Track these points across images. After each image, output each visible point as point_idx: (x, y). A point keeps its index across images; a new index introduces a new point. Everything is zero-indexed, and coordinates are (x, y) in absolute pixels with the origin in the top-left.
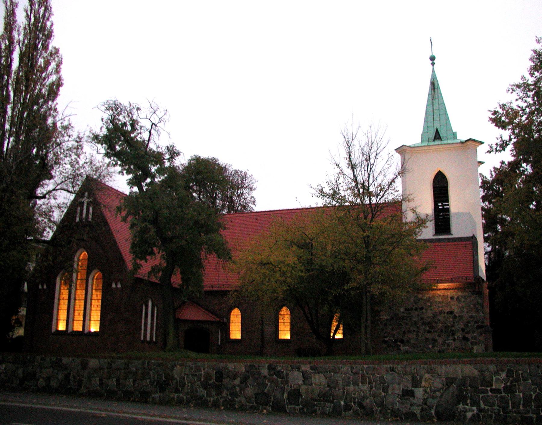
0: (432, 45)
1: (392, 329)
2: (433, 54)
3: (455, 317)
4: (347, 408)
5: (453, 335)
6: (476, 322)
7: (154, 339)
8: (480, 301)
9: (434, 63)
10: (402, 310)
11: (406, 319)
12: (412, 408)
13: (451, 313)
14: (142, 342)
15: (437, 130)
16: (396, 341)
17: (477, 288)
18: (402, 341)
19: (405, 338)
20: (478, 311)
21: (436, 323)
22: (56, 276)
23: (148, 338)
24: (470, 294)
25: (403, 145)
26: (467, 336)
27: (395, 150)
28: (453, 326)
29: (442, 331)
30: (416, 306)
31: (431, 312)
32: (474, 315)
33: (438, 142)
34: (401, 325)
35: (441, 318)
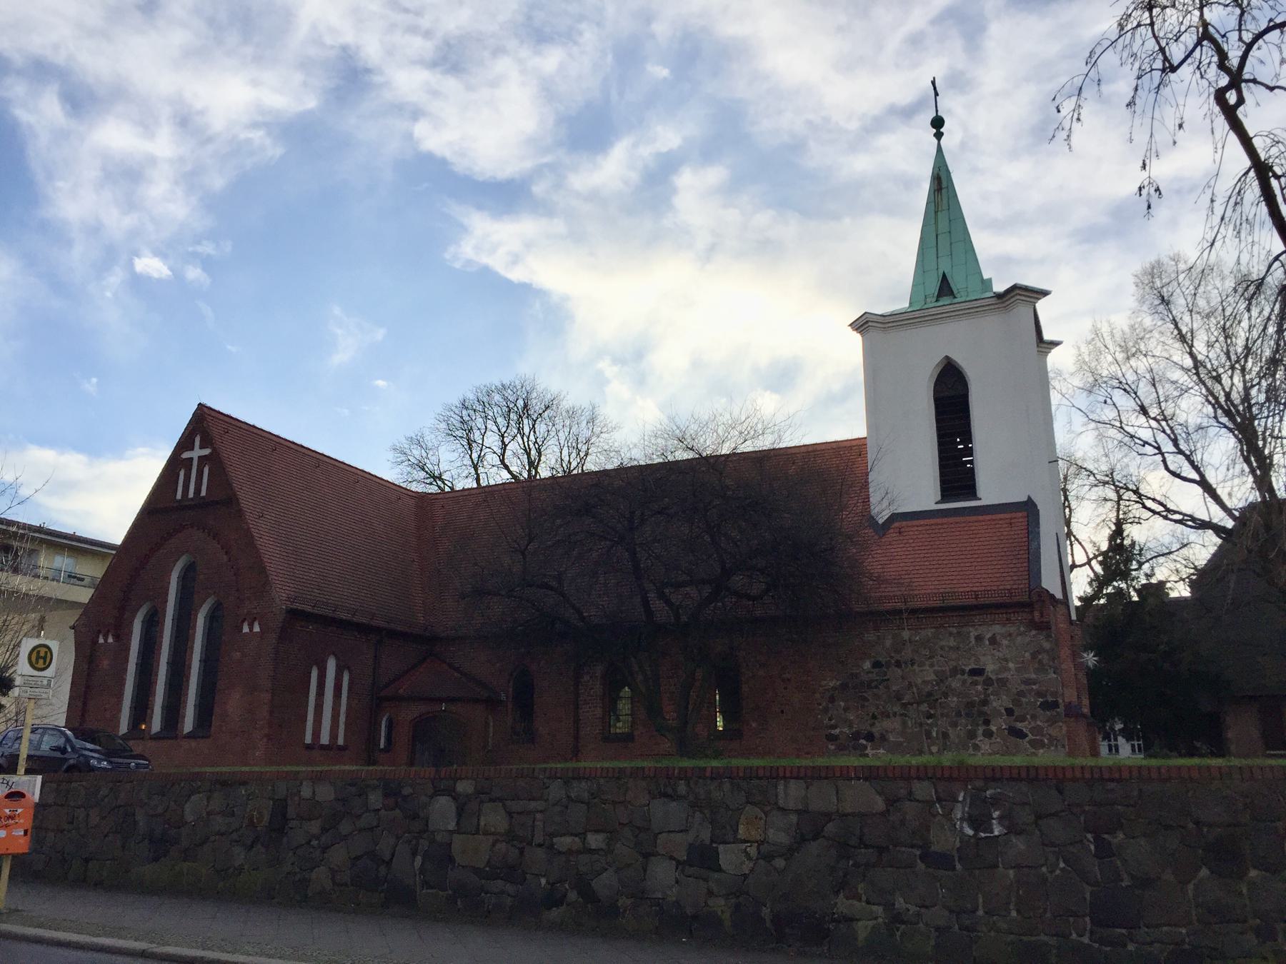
0: (1058, 540)
1: (846, 709)
2: (939, 114)
3: (988, 682)
4: (553, 900)
5: (987, 722)
6: (1039, 694)
7: (341, 741)
8: (1047, 645)
9: (942, 134)
10: (867, 665)
11: (876, 687)
12: (710, 902)
13: (977, 672)
14: (309, 747)
15: (944, 275)
16: (856, 736)
17: (1037, 614)
18: (870, 737)
19: (876, 730)
20: (1041, 668)
21: (946, 695)
22: (134, 617)
23: (325, 739)
24: (1022, 629)
25: (866, 313)
26: (1019, 725)
27: (850, 325)
28: (985, 702)
29: (959, 714)
30: (898, 657)
31: (931, 670)
32: (1033, 676)
33: (946, 300)
34: (866, 699)
35: (955, 683)
